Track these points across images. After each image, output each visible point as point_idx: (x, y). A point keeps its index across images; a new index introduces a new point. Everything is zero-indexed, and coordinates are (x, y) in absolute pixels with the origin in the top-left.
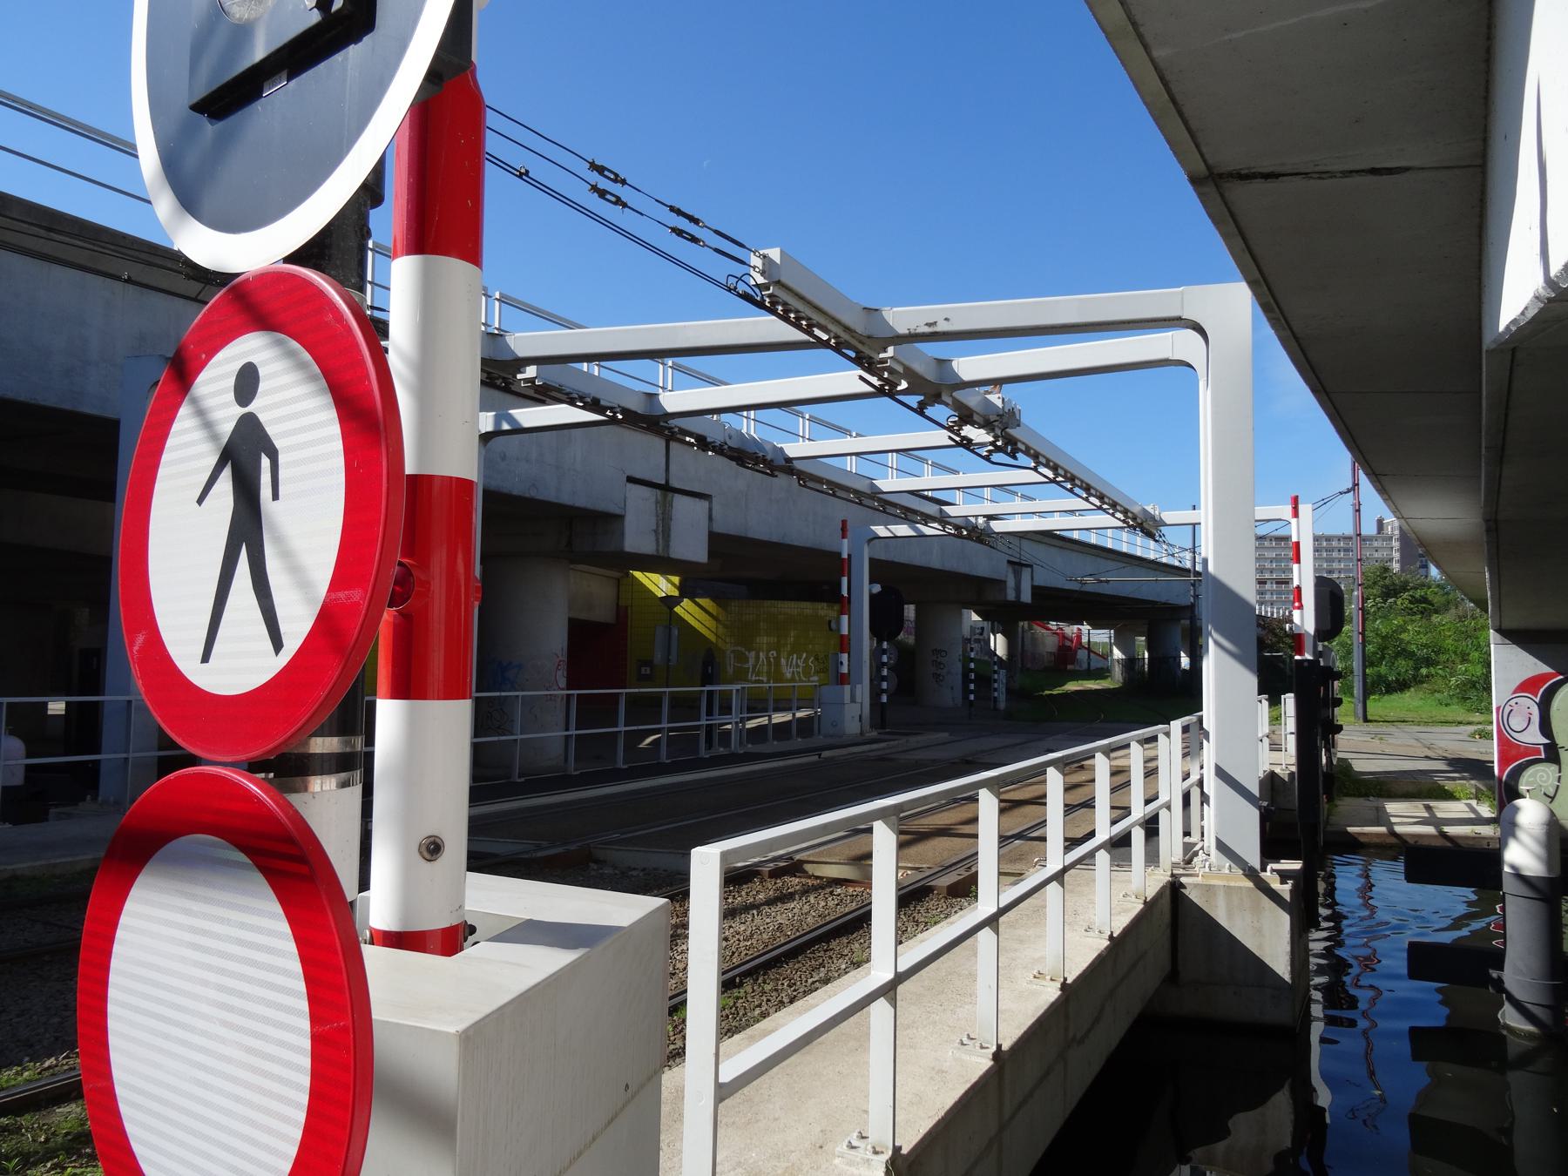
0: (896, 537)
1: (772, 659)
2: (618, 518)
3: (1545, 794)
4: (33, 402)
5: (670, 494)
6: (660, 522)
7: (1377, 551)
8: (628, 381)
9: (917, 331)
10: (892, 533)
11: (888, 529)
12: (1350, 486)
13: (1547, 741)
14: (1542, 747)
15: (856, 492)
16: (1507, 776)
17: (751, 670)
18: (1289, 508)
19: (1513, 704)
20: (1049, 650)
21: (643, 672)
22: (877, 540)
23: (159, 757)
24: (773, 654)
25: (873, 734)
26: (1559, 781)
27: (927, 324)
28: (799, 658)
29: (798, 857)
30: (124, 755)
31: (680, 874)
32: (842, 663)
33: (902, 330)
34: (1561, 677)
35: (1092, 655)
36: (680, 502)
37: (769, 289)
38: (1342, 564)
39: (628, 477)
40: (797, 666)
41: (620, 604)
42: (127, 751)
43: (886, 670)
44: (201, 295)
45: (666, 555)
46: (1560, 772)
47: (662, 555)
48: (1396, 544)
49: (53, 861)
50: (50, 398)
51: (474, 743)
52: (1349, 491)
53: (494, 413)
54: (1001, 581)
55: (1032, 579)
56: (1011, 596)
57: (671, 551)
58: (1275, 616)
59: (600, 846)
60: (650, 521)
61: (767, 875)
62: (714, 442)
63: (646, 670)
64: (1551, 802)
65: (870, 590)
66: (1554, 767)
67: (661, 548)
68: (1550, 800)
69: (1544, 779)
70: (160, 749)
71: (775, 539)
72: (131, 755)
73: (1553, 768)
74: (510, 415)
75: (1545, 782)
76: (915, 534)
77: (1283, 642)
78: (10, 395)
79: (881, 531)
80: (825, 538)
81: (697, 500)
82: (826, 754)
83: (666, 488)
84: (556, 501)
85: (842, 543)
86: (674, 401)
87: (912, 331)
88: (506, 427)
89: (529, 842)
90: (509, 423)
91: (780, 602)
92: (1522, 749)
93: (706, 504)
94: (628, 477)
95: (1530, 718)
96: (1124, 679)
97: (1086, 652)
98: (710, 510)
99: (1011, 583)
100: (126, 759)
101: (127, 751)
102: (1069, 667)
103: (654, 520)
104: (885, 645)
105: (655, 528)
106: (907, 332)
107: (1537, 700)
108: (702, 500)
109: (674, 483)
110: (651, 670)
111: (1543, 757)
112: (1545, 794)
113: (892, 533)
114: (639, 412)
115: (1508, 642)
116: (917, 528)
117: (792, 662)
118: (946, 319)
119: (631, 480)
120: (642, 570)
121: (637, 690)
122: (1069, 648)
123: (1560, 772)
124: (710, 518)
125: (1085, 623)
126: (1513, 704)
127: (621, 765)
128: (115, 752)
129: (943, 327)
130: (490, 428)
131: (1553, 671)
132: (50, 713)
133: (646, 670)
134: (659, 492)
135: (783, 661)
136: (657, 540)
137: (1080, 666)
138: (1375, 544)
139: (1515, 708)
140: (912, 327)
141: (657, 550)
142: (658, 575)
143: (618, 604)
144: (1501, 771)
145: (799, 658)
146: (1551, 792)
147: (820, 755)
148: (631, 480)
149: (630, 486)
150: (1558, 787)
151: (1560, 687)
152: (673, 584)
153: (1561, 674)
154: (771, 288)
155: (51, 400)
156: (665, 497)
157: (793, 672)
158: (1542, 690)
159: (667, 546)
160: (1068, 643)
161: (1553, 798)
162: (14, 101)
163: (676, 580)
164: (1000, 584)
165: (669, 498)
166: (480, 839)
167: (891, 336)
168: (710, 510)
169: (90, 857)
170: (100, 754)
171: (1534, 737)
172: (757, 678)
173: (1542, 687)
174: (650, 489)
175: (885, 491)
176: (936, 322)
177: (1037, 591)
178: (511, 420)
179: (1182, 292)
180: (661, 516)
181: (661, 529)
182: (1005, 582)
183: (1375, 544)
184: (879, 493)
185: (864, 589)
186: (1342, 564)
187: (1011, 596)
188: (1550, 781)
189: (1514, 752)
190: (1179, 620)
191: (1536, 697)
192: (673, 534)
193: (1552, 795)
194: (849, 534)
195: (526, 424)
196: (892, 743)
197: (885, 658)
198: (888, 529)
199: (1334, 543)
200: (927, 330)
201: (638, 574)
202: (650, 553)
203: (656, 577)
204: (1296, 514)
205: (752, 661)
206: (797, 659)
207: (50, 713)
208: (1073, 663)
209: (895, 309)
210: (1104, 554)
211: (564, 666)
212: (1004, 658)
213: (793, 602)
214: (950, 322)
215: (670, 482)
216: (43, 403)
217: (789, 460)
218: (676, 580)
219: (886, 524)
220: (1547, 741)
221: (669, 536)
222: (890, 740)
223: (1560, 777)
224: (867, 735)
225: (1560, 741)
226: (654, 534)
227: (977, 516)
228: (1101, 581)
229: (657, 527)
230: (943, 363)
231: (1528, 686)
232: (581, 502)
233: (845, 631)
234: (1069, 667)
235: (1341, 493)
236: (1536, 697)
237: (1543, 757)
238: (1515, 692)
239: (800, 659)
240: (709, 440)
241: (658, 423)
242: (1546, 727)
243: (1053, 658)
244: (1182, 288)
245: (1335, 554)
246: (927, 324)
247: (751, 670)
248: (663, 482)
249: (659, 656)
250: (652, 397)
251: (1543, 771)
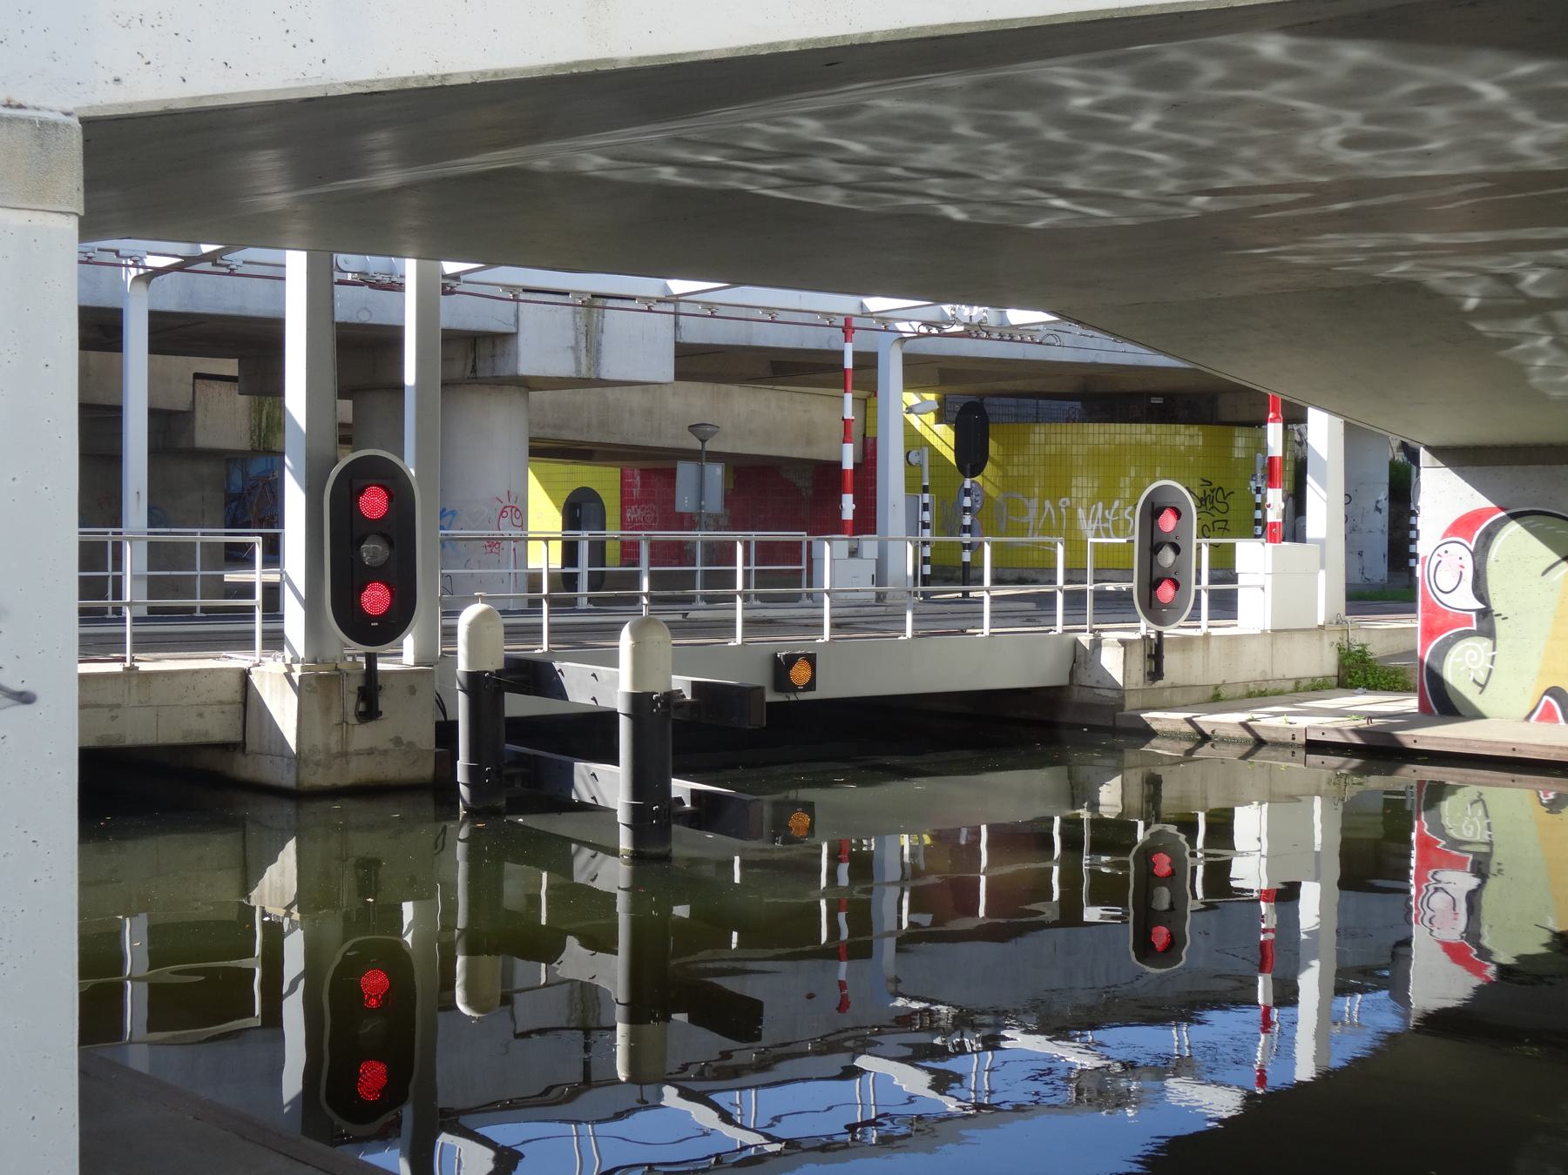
1: (1063, 510)
13: (1481, 606)
14: (1474, 614)
15: (645, 299)
16: (1431, 654)
19: (1442, 553)
24: (1064, 503)
26: (1492, 664)
28: (1108, 507)
35: (1225, 495)
40: (1104, 519)
45: (594, 376)
46: (1494, 650)
51: (121, 571)
64: (1481, 693)
66: (1487, 643)
68: (1480, 689)
69: (1473, 660)
92: (1450, 618)
95: (1461, 573)
103: (570, 334)
105: (573, 343)
107: (1472, 547)
112: (1474, 681)
115: (1439, 463)
123: (1494, 650)
126: (1442, 553)
131: (1493, 506)
132: (225, 580)
135: (1081, 513)
139: (1445, 559)
141: (578, 371)
143: (864, 435)
144: (1424, 648)
145: (1108, 507)
146: (1482, 679)
150: (1490, 670)
151: (1502, 526)
161: (1483, 687)
170: (692, 682)
171: (1464, 600)
173: (1478, 528)
180: (583, 329)
181: (583, 344)
189: (1438, 622)
191: (1470, 542)
193: (1482, 682)
206: (1104, 509)
207: (225, 580)
220: (1481, 606)
223: (1493, 656)
225: (1497, 606)
229: (577, 342)
231: (1462, 526)
236: (1470, 543)
238: (1445, 536)
239: (1110, 509)
251: (1474, 648)
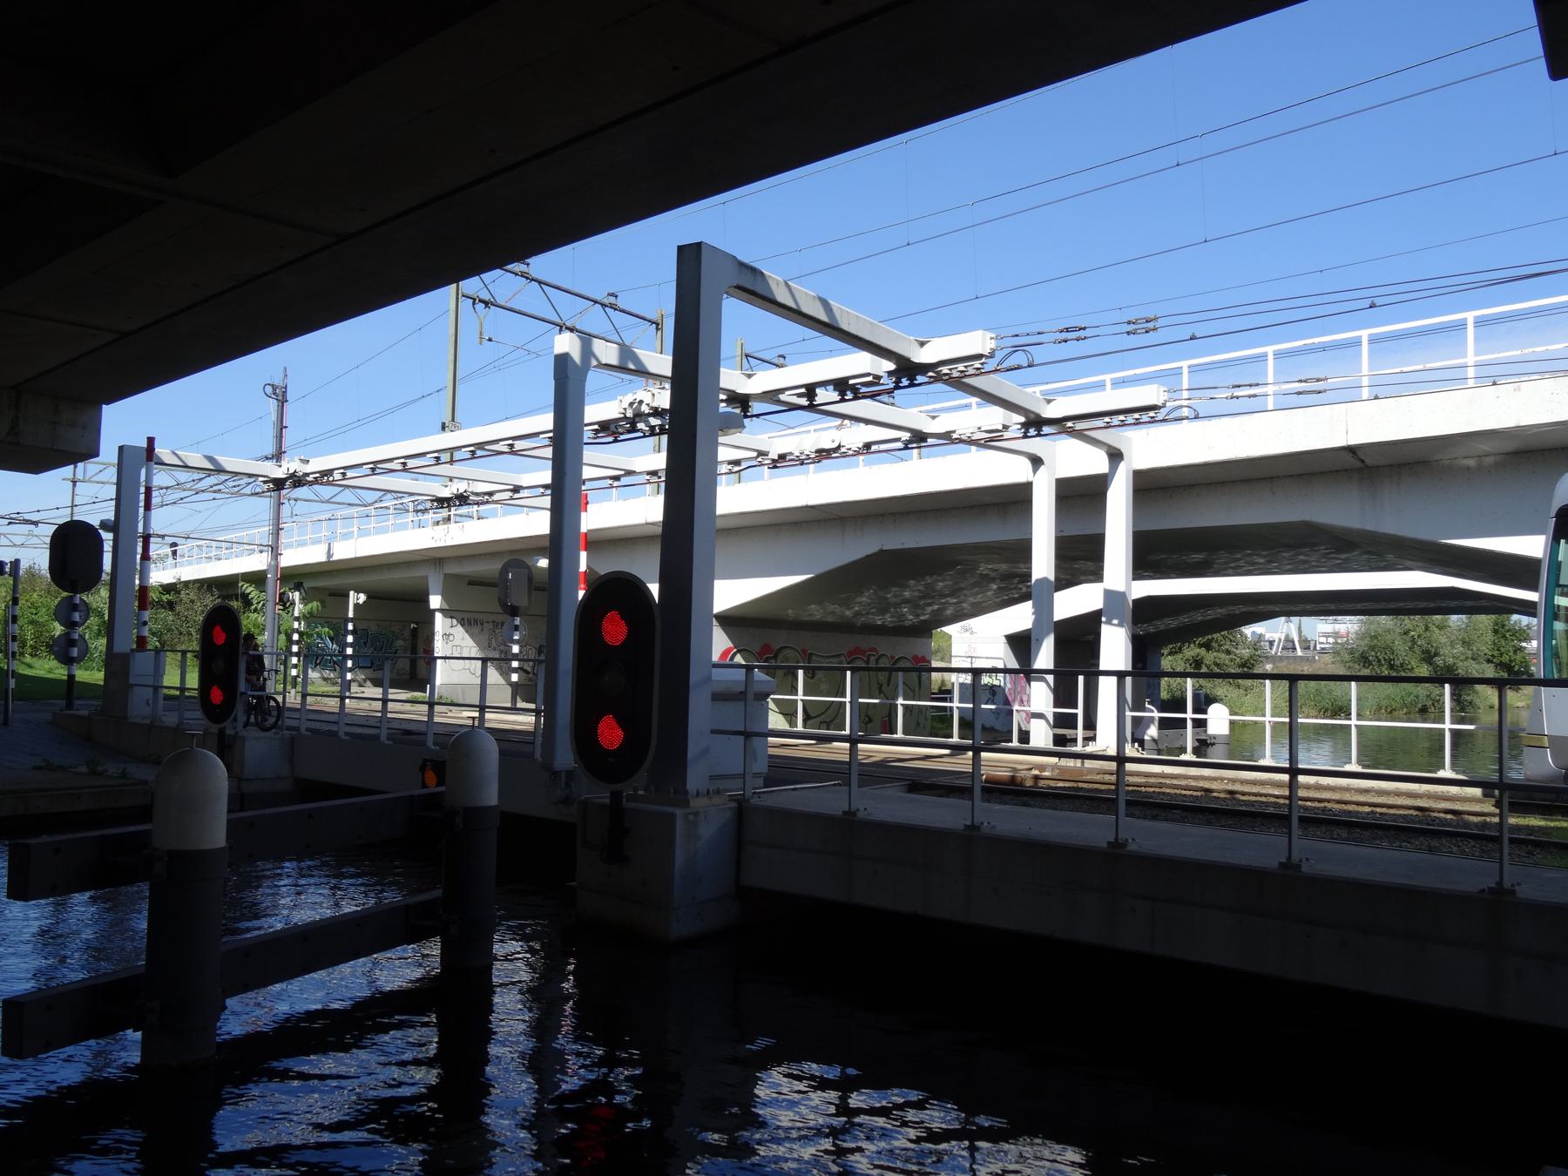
116: (213, 464)
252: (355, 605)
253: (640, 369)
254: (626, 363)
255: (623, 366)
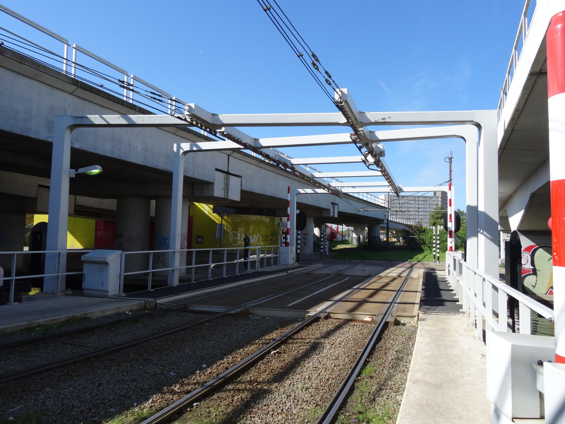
0: (307, 193)
2: (212, 184)
3: (532, 285)
4: (12, 132)
5: (229, 175)
6: (225, 186)
7: (434, 201)
8: (249, 133)
9: (378, 121)
10: (306, 192)
11: (304, 190)
12: (449, 180)
13: (533, 268)
14: (531, 270)
17: (239, 240)
18: (448, 187)
20: (328, 234)
21: (198, 240)
22: (299, 194)
23: (67, 275)
25: (296, 264)
27: (382, 119)
29: (328, 311)
30: (58, 274)
31: (284, 318)
32: (287, 238)
33: (373, 120)
34: (538, 246)
36: (232, 178)
37: (342, 103)
38: (423, 206)
39: (216, 168)
40: (255, 239)
41: (190, 215)
42: (58, 272)
43: (299, 241)
44: (74, 93)
45: (227, 198)
46: (537, 278)
47: (226, 198)
48: (440, 199)
49: (52, 318)
50: (18, 131)
52: (448, 181)
53: (190, 143)
54: (329, 209)
55: (338, 209)
56: (332, 215)
57: (229, 197)
58: (404, 223)
59: (251, 308)
60: (222, 186)
61: (323, 318)
62: (273, 158)
63: (200, 240)
65: (296, 212)
66: (535, 276)
67: (225, 195)
70: (67, 272)
71: (261, 193)
72: (60, 274)
73: (534, 277)
74: (197, 144)
75: (532, 281)
76: (314, 192)
77: (416, 232)
78: (3, 128)
79: (301, 191)
80: (283, 195)
81: (237, 178)
82: (289, 272)
83: (227, 173)
84: (192, 177)
85: (288, 196)
86: (264, 142)
87: (377, 121)
88: (195, 149)
89: (299, 310)
90: (196, 147)
91: (250, 215)
93: (240, 179)
94: (216, 168)
96: (358, 245)
97: (341, 236)
98: (241, 181)
99: (332, 210)
100: (58, 276)
101: (58, 272)
102: (335, 240)
103: (224, 184)
104: (299, 232)
105: (224, 188)
106: (375, 121)
107: (530, 254)
108: (239, 178)
109: (231, 172)
110: (197, 240)
111: (532, 273)
112: (532, 285)
113: (306, 192)
114: (252, 145)
117: (254, 237)
118: (389, 117)
119: (217, 170)
120: (198, 202)
121: (230, 248)
122: (334, 233)
123: (537, 278)
124: (241, 185)
125: (344, 225)
127: (225, 276)
128: (51, 273)
129: (388, 120)
130: (188, 149)
131: (535, 244)
133: (200, 240)
134: (225, 174)
136: (224, 192)
137: (337, 239)
138: (433, 199)
140: (377, 120)
141: (224, 196)
142: (204, 204)
147: (287, 272)
148: (217, 170)
149: (216, 172)
152: (211, 208)
153: (538, 245)
154: (343, 103)
155: (18, 131)
156: (227, 176)
157: (254, 241)
158: (532, 251)
159: (228, 194)
160: (333, 231)
161: (534, 287)
162: (6, 10)
163: (212, 206)
164: (328, 210)
165: (229, 177)
166: (203, 306)
167: (369, 122)
168: (241, 181)
169: (65, 316)
172: (241, 243)
174: (222, 173)
175: (317, 177)
176: (385, 118)
177: (339, 213)
178: (197, 146)
179: (474, 112)
181: (226, 188)
182: (330, 210)
183: (433, 199)
184: (314, 178)
185: (293, 211)
186: (423, 206)
187: (332, 215)
188: (534, 281)
190: (379, 224)
191: (530, 253)
192: (229, 192)
194: (290, 191)
195: (204, 148)
196: (307, 267)
197: (299, 237)
198: (304, 190)
199: (420, 199)
200: (382, 121)
201: (197, 204)
202: (222, 197)
203: (204, 205)
204: (450, 189)
205: (239, 237)
208: (336, 238)
209: (370, 113)
210: (359, 201)
211: (186, 239)
212: (319, 236)
213: (259, 216)
214: (391, 119)
215: (229, 171)
216: (15, 132)
217: (292, 165)
218: (212, 206)
219: (303, 189)
220: (533, 268)
221: (228, 191)
222: (306, 267)
224: (295, 264)
225: (537, 268)
226: (223, 190)
227: (338, 187)
228: (365, 210)
229: (225, 187)
230: (372, 133)
232: (201, 177)
233: (289, 227)
234: (335, 240)
235: (446, 182)
236: (530, 253)
237: (532, 273)
240: (270, 157)
241: (257, 149)
242: (533, 263)
243: (329, 237)
244: (473, 111)
245: (420, 202)
246: (382, 119)
247: (239, 240)
248: (227, 171)
249: (218, 235)
250: (256, 140)
251: (532, 278)
252: (439, 230)
253: (200, 149)
254: (193, 148)
255: (192, 150)
